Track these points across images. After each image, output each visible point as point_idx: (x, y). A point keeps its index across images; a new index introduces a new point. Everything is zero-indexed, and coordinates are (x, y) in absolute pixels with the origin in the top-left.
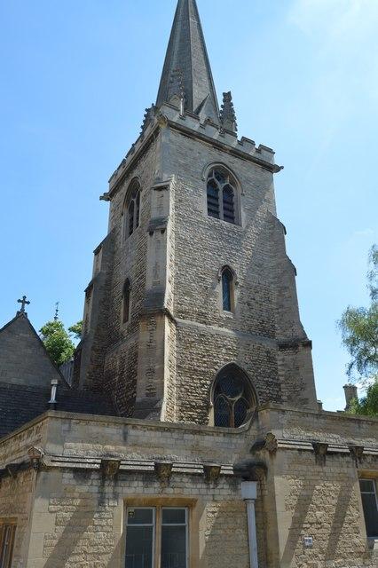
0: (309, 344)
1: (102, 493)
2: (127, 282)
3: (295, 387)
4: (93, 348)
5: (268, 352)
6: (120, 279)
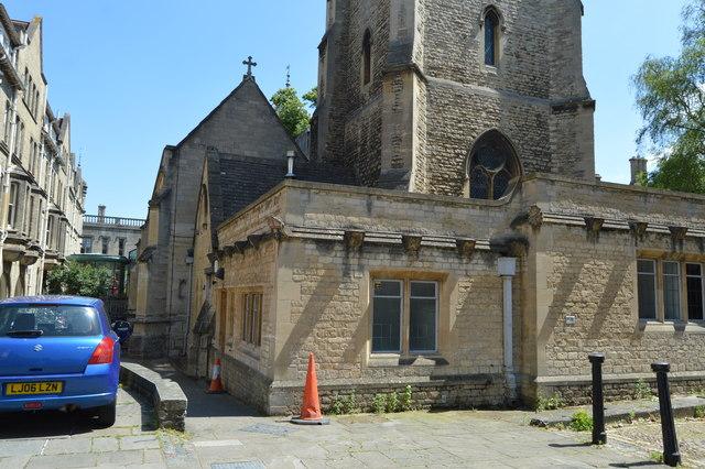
0: (591, 105)
2: (368, 34)
3: (569, 157)
4: (331, 115)
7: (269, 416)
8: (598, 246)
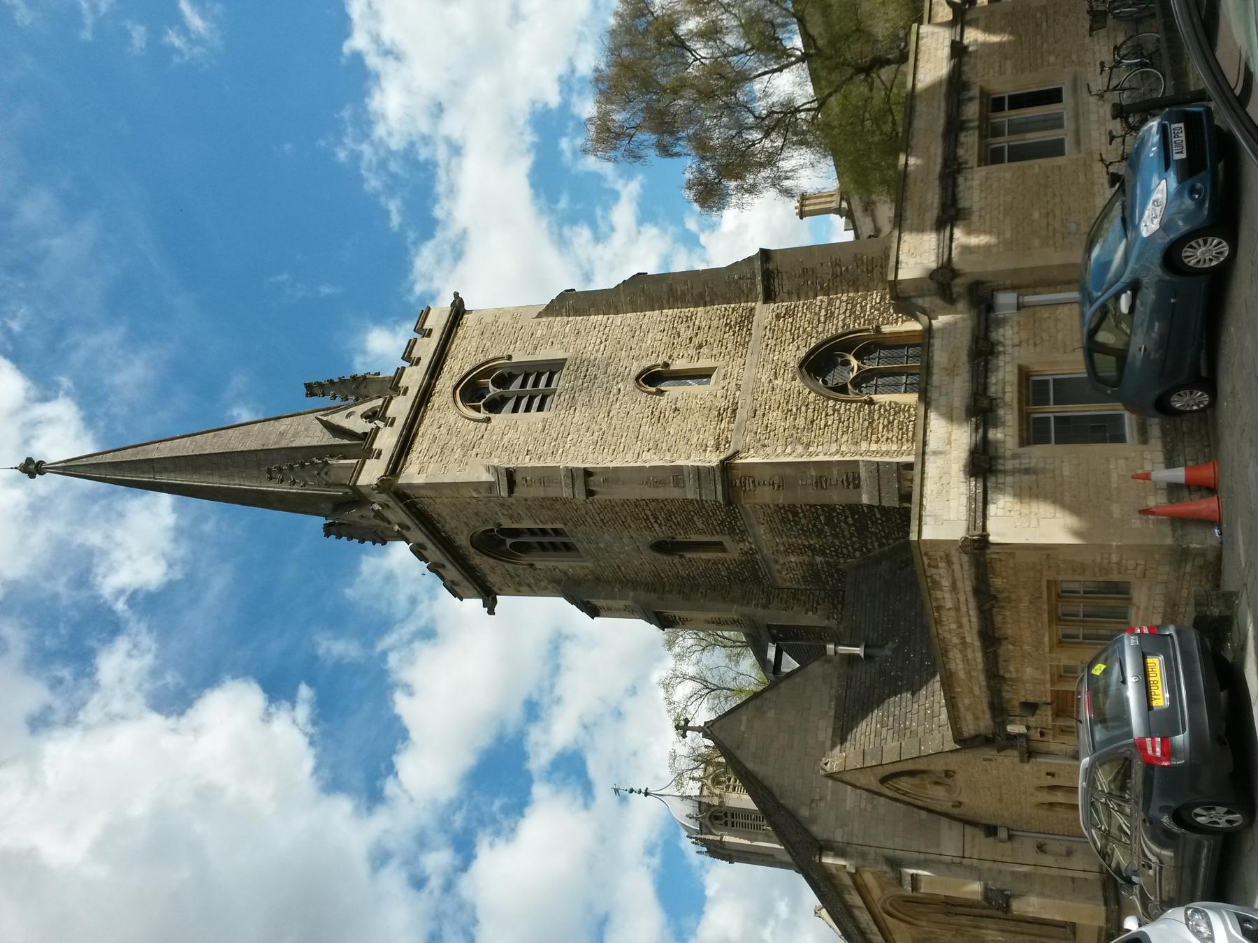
0: (765, 254)
1: (1013, 472)
2: (661, 547)
3: (835, 275)
4: (765, 607)
5: (778, 317)
6: (645, 562)
7: (1222, 553)
8: (975, 207)
